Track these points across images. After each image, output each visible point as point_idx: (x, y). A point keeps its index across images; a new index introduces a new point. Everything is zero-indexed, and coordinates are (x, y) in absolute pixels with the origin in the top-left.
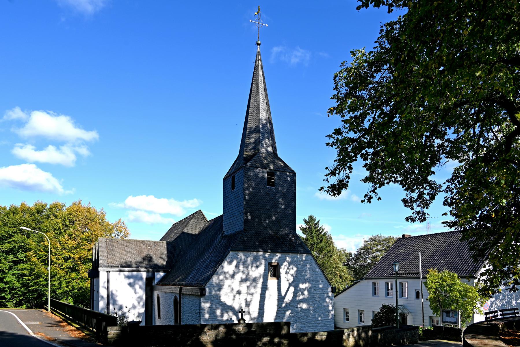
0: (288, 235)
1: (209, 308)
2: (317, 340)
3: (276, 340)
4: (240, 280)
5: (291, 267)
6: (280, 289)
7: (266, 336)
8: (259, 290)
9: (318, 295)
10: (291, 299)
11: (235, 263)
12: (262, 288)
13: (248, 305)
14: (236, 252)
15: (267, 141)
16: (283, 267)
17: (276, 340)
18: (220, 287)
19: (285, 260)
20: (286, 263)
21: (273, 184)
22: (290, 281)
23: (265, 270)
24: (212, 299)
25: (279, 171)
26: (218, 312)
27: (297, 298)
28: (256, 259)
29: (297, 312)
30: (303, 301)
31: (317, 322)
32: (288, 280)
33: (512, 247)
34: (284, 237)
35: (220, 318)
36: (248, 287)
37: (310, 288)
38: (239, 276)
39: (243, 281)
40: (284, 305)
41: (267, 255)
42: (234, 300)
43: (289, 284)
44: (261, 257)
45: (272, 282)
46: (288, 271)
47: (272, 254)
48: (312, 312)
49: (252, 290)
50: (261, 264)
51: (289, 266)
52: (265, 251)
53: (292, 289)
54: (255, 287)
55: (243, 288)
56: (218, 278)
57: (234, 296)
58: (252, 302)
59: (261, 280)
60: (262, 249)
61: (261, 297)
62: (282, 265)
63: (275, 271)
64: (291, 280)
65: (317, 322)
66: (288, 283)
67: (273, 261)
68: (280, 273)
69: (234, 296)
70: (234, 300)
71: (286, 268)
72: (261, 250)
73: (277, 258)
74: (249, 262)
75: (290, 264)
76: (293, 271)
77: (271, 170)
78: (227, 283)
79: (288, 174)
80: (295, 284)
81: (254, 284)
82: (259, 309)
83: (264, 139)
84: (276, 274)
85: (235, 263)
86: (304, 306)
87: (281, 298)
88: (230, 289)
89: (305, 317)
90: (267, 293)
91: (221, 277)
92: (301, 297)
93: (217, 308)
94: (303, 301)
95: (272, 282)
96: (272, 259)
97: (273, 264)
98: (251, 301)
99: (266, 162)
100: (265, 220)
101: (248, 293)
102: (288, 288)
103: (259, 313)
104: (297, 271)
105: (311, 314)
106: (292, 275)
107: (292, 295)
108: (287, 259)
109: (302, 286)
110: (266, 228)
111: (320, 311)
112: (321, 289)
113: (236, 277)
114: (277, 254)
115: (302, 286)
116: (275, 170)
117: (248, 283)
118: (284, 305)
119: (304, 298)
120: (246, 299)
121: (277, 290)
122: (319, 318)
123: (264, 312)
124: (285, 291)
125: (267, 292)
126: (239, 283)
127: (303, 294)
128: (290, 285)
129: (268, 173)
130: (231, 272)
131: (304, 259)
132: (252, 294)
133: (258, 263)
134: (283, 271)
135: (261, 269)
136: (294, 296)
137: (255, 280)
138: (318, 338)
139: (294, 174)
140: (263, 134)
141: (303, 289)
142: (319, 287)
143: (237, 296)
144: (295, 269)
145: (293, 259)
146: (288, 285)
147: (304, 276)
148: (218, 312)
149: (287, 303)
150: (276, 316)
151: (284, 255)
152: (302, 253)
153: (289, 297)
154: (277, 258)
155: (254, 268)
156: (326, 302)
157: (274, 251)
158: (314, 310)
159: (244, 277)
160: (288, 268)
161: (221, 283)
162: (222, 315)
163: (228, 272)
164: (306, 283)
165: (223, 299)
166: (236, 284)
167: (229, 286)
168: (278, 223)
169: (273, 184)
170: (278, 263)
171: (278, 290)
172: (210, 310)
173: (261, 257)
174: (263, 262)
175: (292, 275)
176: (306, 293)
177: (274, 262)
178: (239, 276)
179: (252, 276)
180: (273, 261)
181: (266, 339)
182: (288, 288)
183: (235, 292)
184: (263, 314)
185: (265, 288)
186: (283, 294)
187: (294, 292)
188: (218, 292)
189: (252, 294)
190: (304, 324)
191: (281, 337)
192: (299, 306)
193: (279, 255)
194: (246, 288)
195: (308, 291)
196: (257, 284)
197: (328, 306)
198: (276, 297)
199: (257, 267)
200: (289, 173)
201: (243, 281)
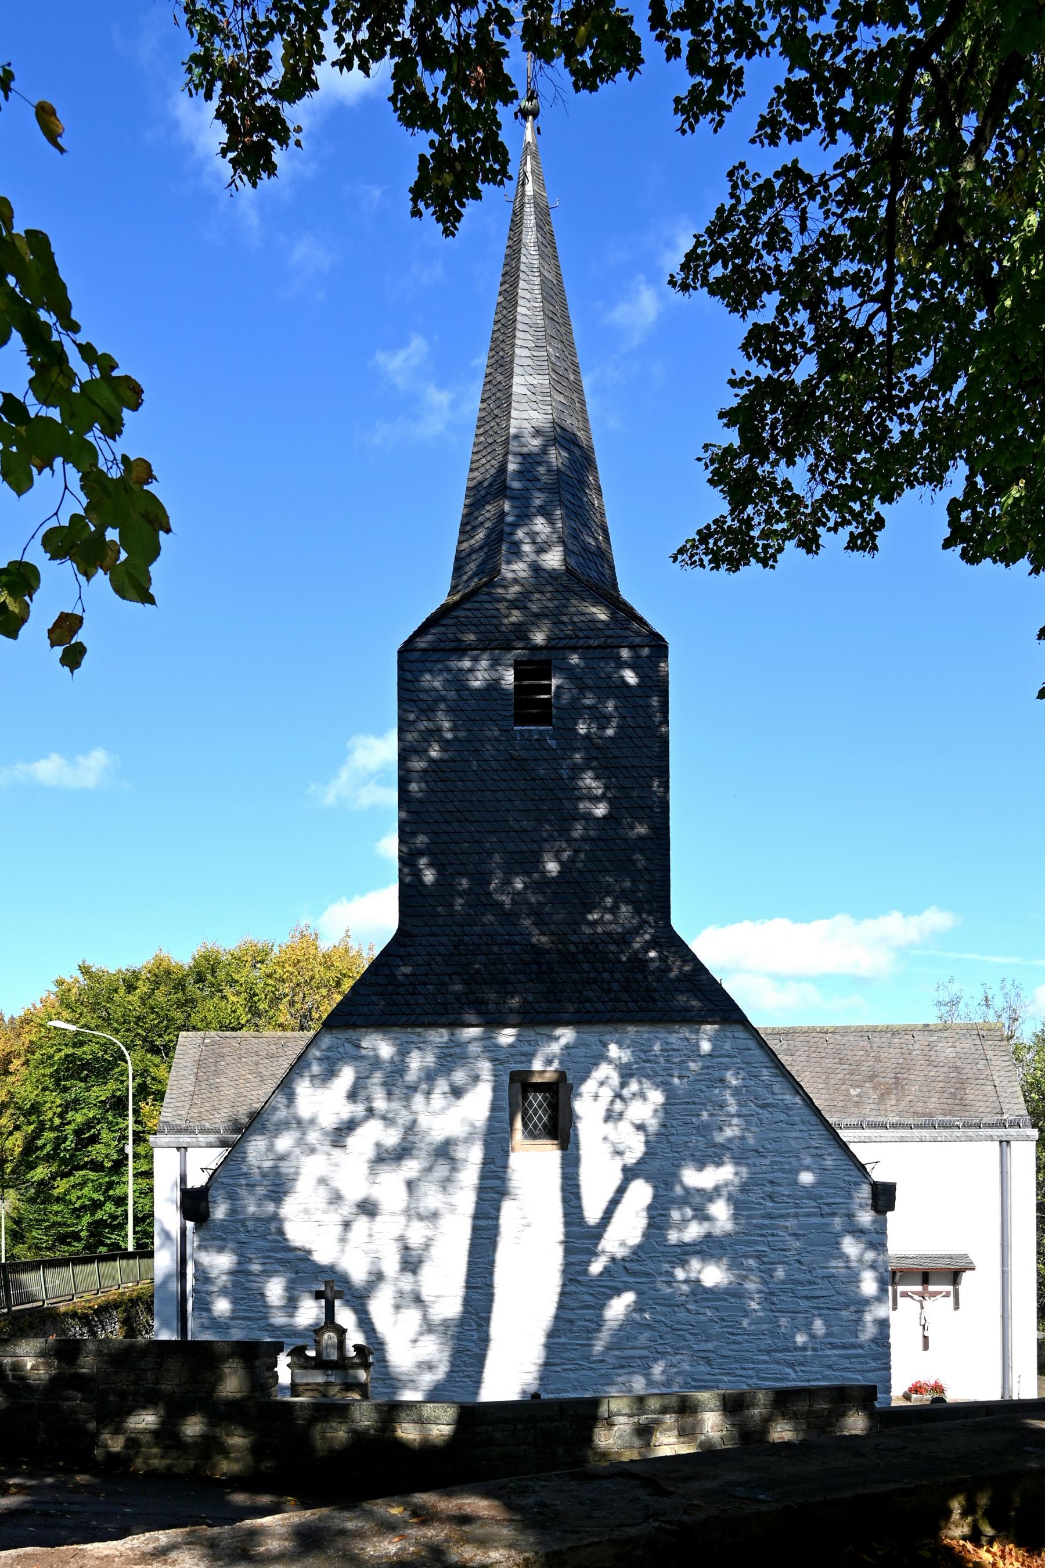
0: (623, 940)
1: (231, 1273)
2: (401, 1446)
3: (193, 1427)
4: (370, 1153)
5: (634, 1086)
6: (578, 1197)
7: (148, 1401)
8: (465, 1199)
9: (791, 1223)
10: (635, 1238)
11: (347, 1076)
12: (481, 1190)
13: (411, 1263)
14: (351, 1034)
15: (540, 525)
16: (588, 1087)
17: (193, 1427)
18: (278, 1186)
19: (601, 1057)
20: (604, 1071)
21: (543, 713)
22: (631, 1158)
23: (494, 1108)
24: (242, 1237)
25: (574, 649)
26: (275, 1290)
27: (673, 1237)
28: (450, 1059)
29: (670, 1303)
30: (709, 1248)
31: (789, 1356)
32: (620, 1153)
33: (969, 453)
34: (598, 951)
35: (279, 1319)
36: (411, 1185)
37: (744, 1188)
38: (372, 1135)
39: (386, 1158)
40: (596, 1267)
41: (507, 1036)
42: (343, 1240)
43: (625, 1169)
44: (475, 1049)
45: (534, 1163)
46: (618, 1106)
47: (530, 1034)
48: (754, 1305)
49: (431, 1198)
50: (476, 1079)
51: (623, 1085)
52: (493, 1022)
53: (641, 1193)
54: (446, 1184)
55: (390, 1188)
56: (270, 1148)
57: (347, 1225)
58: (434, 1251)
59: (474, 1155)
60: (479, 1013)
61: (475, 1229)
62: (583, 1079)
63: (546, 1109)
64: (636, 1148)
65: (789, 1356)
66: (618, 1163)
67: (537, 1065)
68: (571, 1117)
69: (347, 1225)
70: (343, 1240)
71: (607, 1094)
72: (472, 1018)
73: (555, 1048)
74: (411, 1077)
75: (626, 1073)
76: (647, 1106)
77: (537, 648)
78: (310, 1169)
79: (625, 653)
80: (658, 1165)
81: (442, 1170)
82: (469, 1286)
83: (524, 517)
84: (560, 1128)
85: (347, 1076)
86: (713, 1275)
87: (580, 1237)
88: (323, 1193)
89: (717, 1328)
90: (509, 1213)
91: (284, 1143)
92: (694, 1231)
93: (268, 1274)
94: (709, 1248)
95: (534, 1163)
96: (530, 1056)
97: (537, 1079)
98: (427, 1246)
99: (516, 616)
100: (507, 882)
101: (412, 1213)
102: (621, 1190)
103: (467, 1301)
104: (667, 1108)
105: (746, 1313)
106: (640, 1127)
107: (642, 1222)
108: (614, 1051)
109: (693, 1178)
110: (509, 917)
111: (804, 1304)
112: (809, 1192)
113: (351, 1141)
114: (559, 1031)
115: (693, 1178)
116: (556, 646)
117: (411, 1167)
118: (596, 1267)
119: (709, 1236)
120: (401, 1238)
121: (557, 1195)
122: (800, 1339)
123: (490, 1298)
124: (603, 1205)
125: (507, 1208)
126: (364, 1168)
127: (703, 1216)
128: (630, 1174)
129: (517, 665)
130: (329, 1120)
131: (706, 1046)
132: (434, 1216)
133: (459, 1076)
134: (589, 1107)
135: (478, 1103)
136: (650, 1226)
137: (445, 1152)
138: (408, 1432)
139: (659, 647)
140: (522, 501)
141: (700, 1191)
142: (795, 1183)
143: (362, 1223)
144: (657, 1097)
145: (642, 1051)
146: (617, 1177)
147: (705, 1130)
148: (275, 1290)
149: (613, 1259)
150: (557, 1317)
151: (591, 1034)
152: (694, 1019)
153: (626, 1231)
154: (555, 1048)
155: (437, 1100)
156: (845, 1258)
157: (538, 1018)
158: (768, 1296)
159: (392, 1138)
160: (618, 1096)
161: (286, 1168)
162: (291, 1304)
163: (312, 1121)
164: (719, 1164)
165: (297, 1234)
166: (351, 1169)
167: (322, 1181)
168: (575, 891)
169: (543, 713)
170: (562, 1075)
171: (565, 1201)
172: (235, 1284)
173: (475, 1049)
174: (485, 1067)
175: (640, 1127)
176: (720, 1211)
177: (541, 1068)
178: (372, 1135)
179: (426, 1133)
180: (537, 1065)
181: (146, 1420)
182: (621, 1190)
183: (346, 1209)
184: (489, 1310)
185: (494, 1188)
186: (592, 1213)
187: (650, 1208)
188: (270, 1208)
189: (434, 1216)
190: (708, 1361)
191: (223, 1415)
192: (680, 1274)
193: (566, 1035)
194: (403, 1190)
195: (730, 1198)
196: (454, 1169)
197: (855, 1279)
198: (557, 1230)
199: (457, 1092)
200: (632, 647)
201: (386, 1158)
